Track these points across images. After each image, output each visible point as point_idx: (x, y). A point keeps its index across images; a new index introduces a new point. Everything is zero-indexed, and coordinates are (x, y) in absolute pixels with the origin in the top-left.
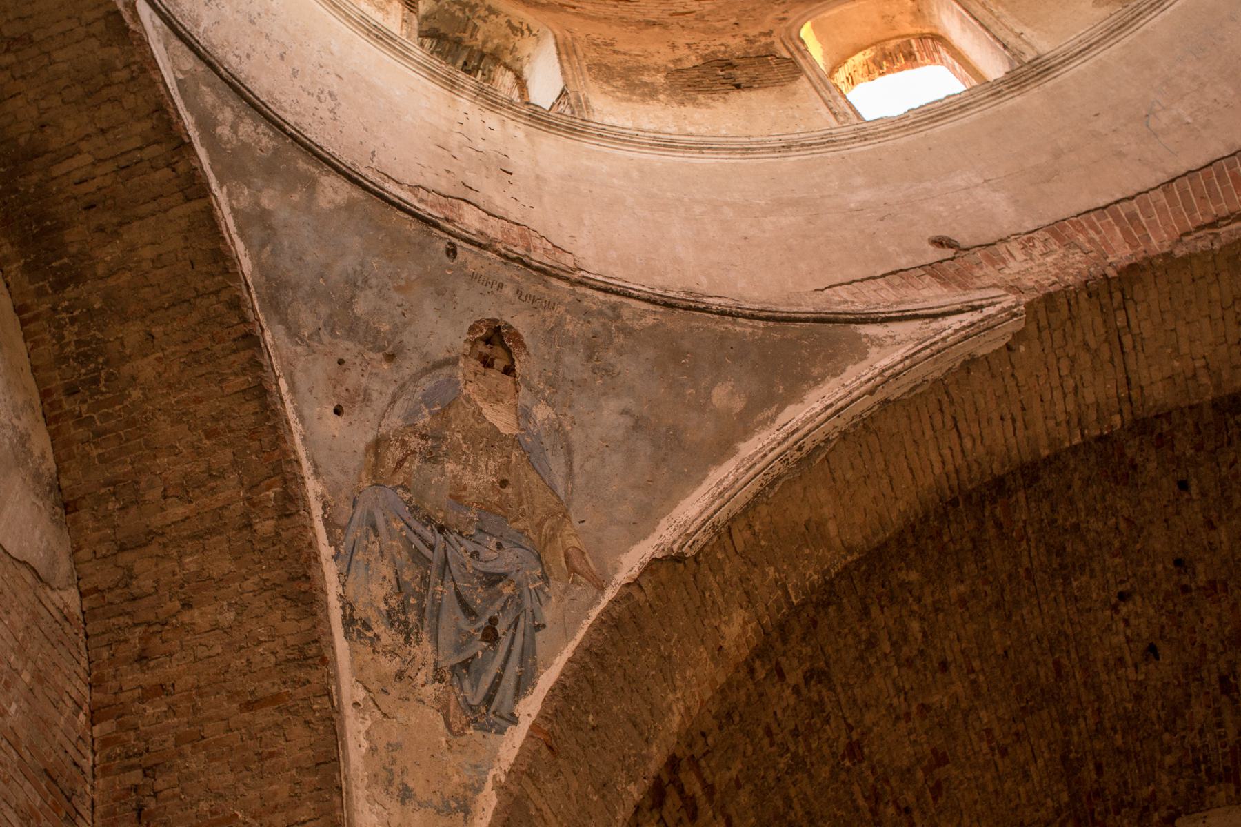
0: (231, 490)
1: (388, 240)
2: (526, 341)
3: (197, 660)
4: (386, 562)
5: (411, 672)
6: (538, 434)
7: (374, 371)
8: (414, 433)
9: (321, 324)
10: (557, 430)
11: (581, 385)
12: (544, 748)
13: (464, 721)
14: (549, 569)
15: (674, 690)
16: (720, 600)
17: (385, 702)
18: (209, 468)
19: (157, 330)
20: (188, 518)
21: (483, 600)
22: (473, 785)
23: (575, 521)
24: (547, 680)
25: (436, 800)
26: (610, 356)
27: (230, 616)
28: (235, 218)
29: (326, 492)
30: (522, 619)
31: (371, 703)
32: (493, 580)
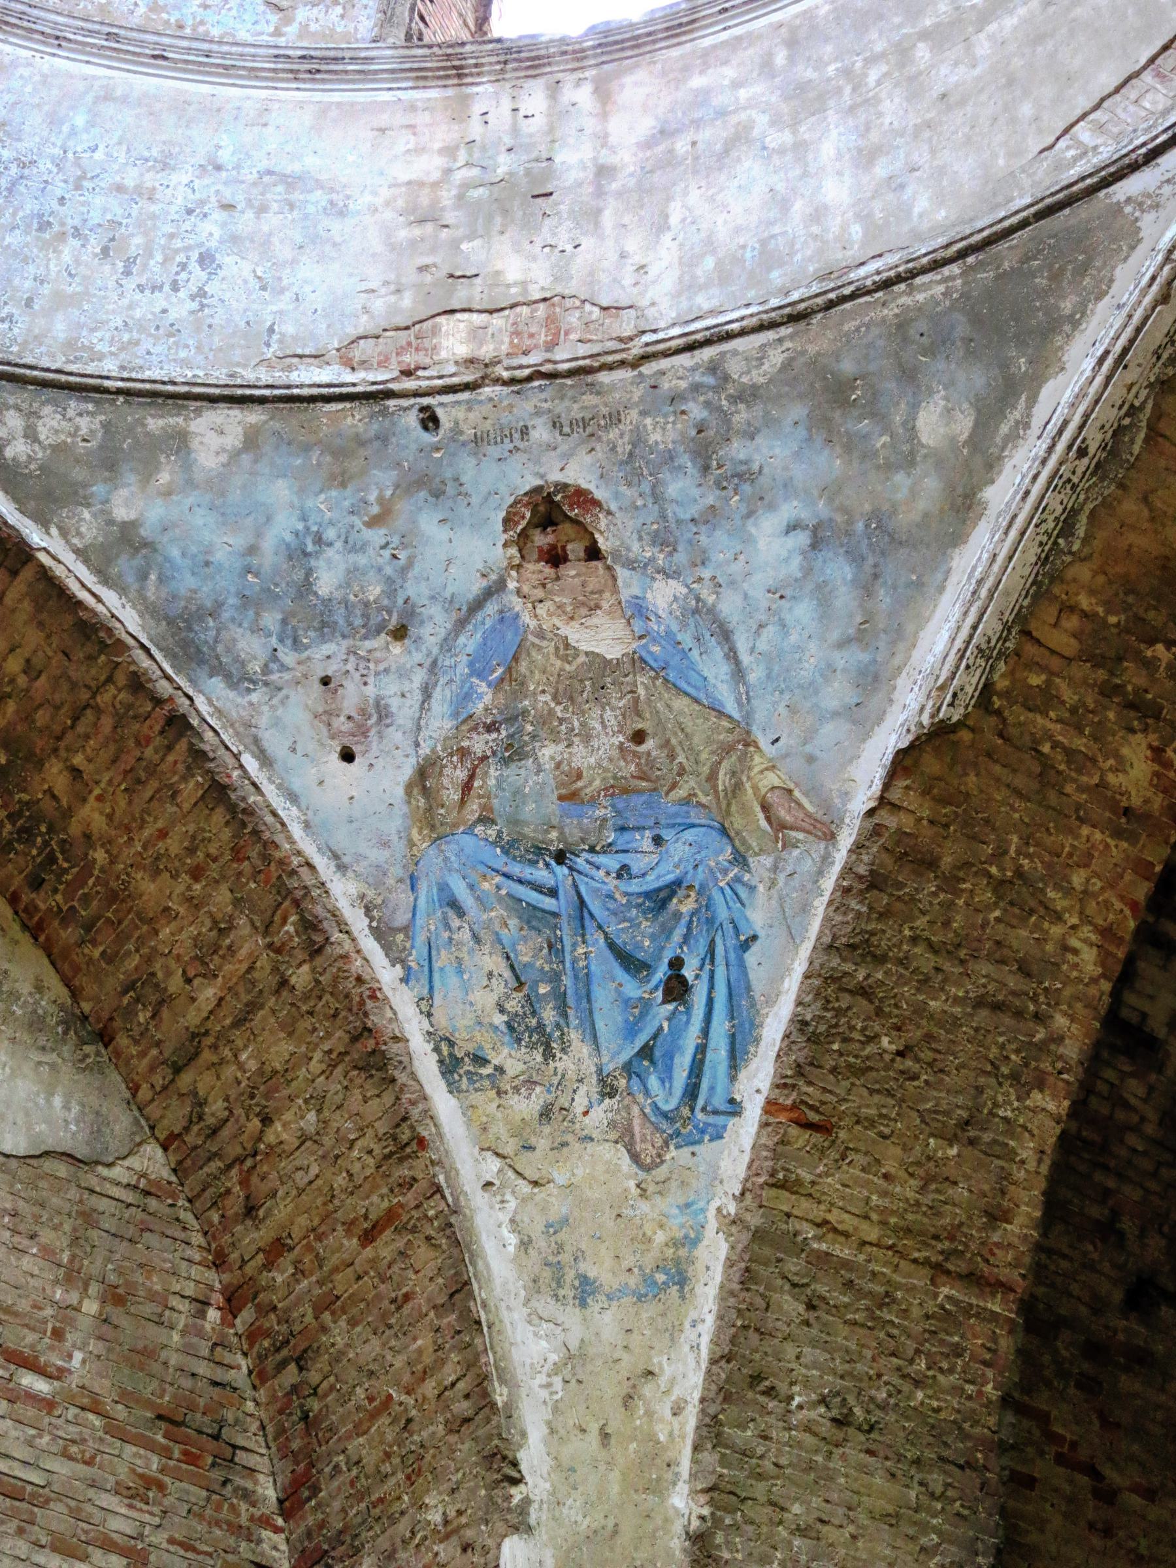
0: (248, 942)
1: (328, 459)
2: (599, 494)
3: (301, 1191)
4: (487, 948)
5: (564, 1101)
6: (669, 634)
7: (381, 667)
8: (475, 729)
9: (274, 641)
10: (696, 611)
11: (710, 517)
12: (794, 1131)
13: (659, 1142)
14: (744, 842)
15: (1058, 917)
16: (1080, 743)
17: (530, 1164)
18: (215, 923)
19: (78, 760)
20: (221, 999)
21: (653, 938)
22: (686, 1237)
23: (764, 742)
24: (774, 1026)
25: (633, 1281)
26: (738, 450)
27: (312, 1116)
28: (86, 562)
29: (363, 888)
30: (719, 941)
31: (510, 1174)
32: (660, 900)
